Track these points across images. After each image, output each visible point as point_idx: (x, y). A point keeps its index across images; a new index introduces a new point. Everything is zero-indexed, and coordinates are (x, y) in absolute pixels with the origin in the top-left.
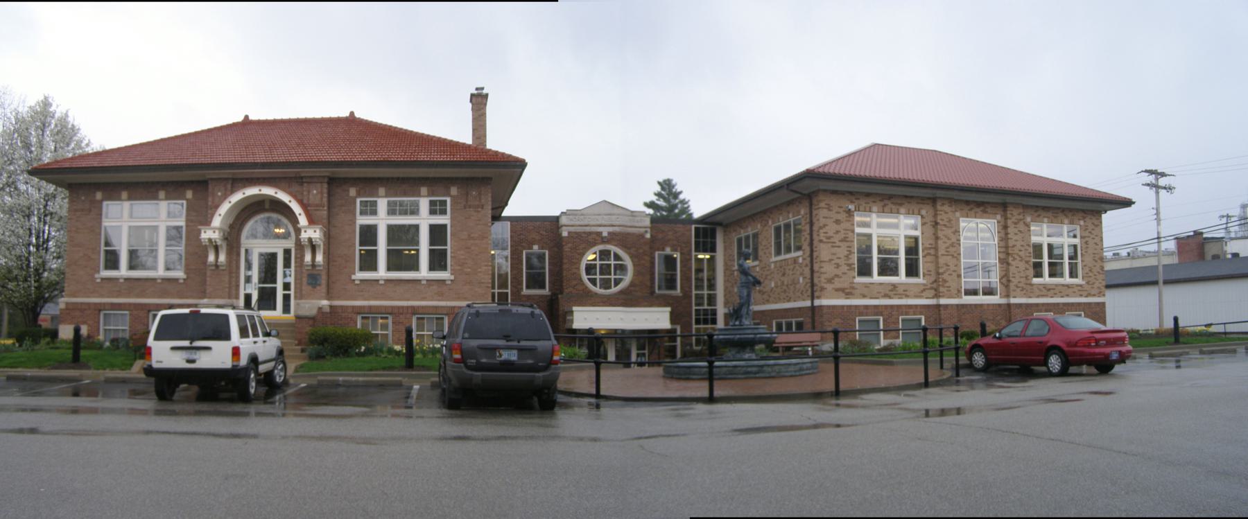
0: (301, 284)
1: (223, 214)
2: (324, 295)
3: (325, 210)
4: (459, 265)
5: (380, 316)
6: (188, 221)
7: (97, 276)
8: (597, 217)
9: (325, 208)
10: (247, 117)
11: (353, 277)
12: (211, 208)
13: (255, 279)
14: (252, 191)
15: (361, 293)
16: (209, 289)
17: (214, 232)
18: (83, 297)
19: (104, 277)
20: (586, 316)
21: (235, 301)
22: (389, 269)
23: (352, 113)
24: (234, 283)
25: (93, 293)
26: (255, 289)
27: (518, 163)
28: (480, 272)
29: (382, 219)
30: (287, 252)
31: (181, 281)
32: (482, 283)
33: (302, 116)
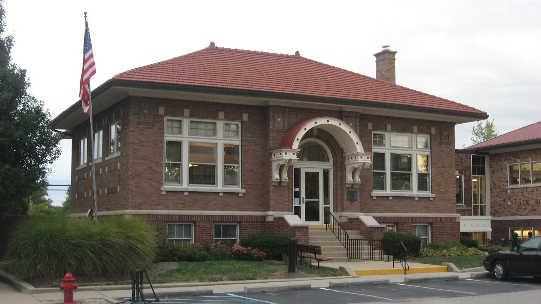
2: (359, 208)
4: (437, 187)
10: (212, 44)
12: (273, 132)
13: (303, 194)
15: (377, 207)
16: (272, 203)
17: (294, 154)
19: (169, 190)
20: (471, 223)
23: (297, 53)
25: (158, 205)
26: (303, 202)
28: (450, 192)
29: (388, 149)
30: (326, 173)
31: (241, 195)
32: (451, 200)
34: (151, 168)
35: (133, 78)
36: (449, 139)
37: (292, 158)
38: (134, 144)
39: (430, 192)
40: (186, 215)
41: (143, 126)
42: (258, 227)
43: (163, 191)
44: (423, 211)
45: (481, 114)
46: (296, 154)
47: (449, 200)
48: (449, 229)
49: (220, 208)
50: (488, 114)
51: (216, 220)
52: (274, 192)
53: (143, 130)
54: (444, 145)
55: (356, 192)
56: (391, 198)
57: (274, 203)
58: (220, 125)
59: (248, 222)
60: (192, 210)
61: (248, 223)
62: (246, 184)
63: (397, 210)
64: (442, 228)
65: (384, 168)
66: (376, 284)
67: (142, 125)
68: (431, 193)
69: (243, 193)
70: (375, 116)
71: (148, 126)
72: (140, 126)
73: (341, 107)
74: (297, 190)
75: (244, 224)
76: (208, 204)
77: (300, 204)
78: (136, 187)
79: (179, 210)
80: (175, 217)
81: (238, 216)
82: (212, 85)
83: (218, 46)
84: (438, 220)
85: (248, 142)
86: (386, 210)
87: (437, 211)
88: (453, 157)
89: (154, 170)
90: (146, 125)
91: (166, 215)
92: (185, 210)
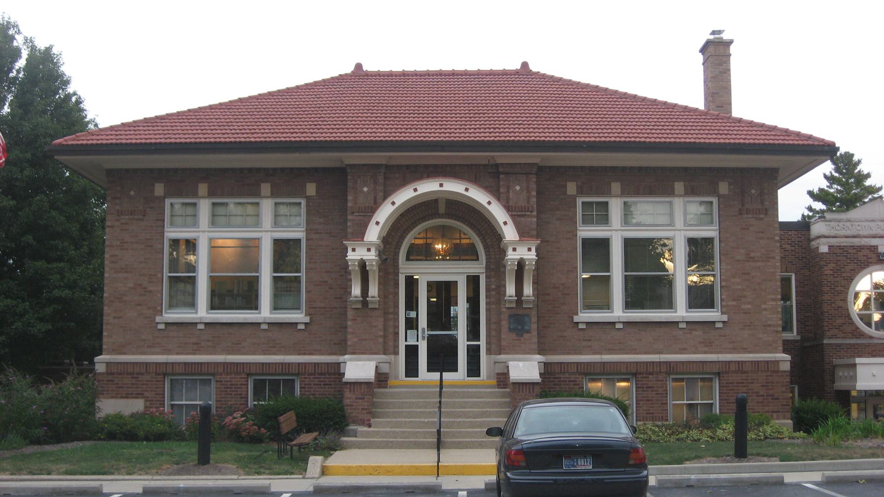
0: (499, 331)
1: (382, 222)
2: (535, 346)
3: (533, 216)
5: (617, 377)
6: (308, 231)
7: (158, 319)
8: (869, 223)
9: (535, 213)
10: (359, 66)
11: (576, 319)
13: (423, 322)
14: (428, 187)
15: (589, 343)
16: (351, 340)
17: (369, 250)
18: (133, 354)
19: (170, 321)
21: (393, 357)
22: (213, 307)
23: (525, 65)
24: (391, 330)
25: (151, 347)
26: (423, 338)
27: (826, 148)
28: (765, 309)
30: (473, 281)
32: (770, 326)
33: (447, 67)
34: (141, 285)
35: (778, 140)
36: (762, 203)
37: (525, 257)
38: (113, 247)
39: (718, 312)
40: (198, 363)
41: (127, 217)
42: (333, 383)
43: (160, 323)
44: (700, 349)
45: (819, 145)
46: (533, 249)
47: (764, 326)
48: (762, 386)
49: (263, 351)
50: (837, 146)
51: (271, 372)
52: (356, 320)
53: (127, 224)
54: (750, 216)
55: (528, 315)
56: (619, 326)
57: (355, 340)
58: (267, 206)
59: (311, 374)
60: (211, 354)
61: (312, 377)
62: (312, 308)
63: (635, 349)
64: (743, 383)
65: (607, 267)
66: (236, 492)
67: (125, 215)
68: (720, 314)
69: (306, 324)
70: (582, 168)
71: (136, 217)
72: (123, 217)
73: (493, 157)
74: (413, 314)
75: (305, 378)
76: (240, 344)
77: (418, 341)
78: (115, 318)
79: (188, 354)
80: (177, 367)
81: (292, 363)
82: (108, 140)
83: (370, 69)
84: (733, 368)
85: (315, 233)
86: (609, 350)
87: (735, 349)
88: (773, 238)
89: (145, 288)
90: (131, 214)
91: (163, 363)
92: (199, 354)
